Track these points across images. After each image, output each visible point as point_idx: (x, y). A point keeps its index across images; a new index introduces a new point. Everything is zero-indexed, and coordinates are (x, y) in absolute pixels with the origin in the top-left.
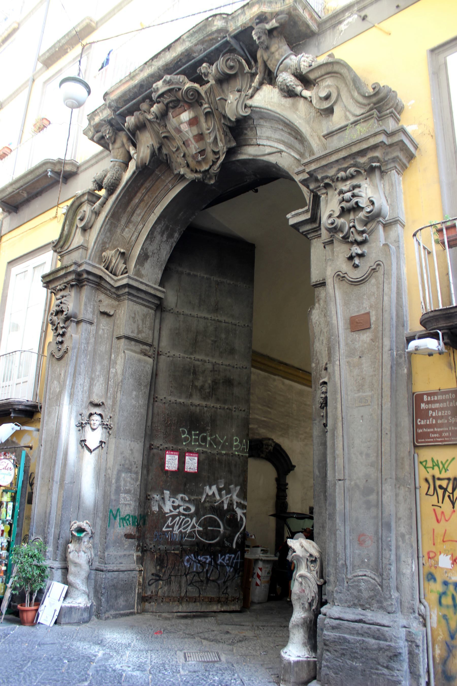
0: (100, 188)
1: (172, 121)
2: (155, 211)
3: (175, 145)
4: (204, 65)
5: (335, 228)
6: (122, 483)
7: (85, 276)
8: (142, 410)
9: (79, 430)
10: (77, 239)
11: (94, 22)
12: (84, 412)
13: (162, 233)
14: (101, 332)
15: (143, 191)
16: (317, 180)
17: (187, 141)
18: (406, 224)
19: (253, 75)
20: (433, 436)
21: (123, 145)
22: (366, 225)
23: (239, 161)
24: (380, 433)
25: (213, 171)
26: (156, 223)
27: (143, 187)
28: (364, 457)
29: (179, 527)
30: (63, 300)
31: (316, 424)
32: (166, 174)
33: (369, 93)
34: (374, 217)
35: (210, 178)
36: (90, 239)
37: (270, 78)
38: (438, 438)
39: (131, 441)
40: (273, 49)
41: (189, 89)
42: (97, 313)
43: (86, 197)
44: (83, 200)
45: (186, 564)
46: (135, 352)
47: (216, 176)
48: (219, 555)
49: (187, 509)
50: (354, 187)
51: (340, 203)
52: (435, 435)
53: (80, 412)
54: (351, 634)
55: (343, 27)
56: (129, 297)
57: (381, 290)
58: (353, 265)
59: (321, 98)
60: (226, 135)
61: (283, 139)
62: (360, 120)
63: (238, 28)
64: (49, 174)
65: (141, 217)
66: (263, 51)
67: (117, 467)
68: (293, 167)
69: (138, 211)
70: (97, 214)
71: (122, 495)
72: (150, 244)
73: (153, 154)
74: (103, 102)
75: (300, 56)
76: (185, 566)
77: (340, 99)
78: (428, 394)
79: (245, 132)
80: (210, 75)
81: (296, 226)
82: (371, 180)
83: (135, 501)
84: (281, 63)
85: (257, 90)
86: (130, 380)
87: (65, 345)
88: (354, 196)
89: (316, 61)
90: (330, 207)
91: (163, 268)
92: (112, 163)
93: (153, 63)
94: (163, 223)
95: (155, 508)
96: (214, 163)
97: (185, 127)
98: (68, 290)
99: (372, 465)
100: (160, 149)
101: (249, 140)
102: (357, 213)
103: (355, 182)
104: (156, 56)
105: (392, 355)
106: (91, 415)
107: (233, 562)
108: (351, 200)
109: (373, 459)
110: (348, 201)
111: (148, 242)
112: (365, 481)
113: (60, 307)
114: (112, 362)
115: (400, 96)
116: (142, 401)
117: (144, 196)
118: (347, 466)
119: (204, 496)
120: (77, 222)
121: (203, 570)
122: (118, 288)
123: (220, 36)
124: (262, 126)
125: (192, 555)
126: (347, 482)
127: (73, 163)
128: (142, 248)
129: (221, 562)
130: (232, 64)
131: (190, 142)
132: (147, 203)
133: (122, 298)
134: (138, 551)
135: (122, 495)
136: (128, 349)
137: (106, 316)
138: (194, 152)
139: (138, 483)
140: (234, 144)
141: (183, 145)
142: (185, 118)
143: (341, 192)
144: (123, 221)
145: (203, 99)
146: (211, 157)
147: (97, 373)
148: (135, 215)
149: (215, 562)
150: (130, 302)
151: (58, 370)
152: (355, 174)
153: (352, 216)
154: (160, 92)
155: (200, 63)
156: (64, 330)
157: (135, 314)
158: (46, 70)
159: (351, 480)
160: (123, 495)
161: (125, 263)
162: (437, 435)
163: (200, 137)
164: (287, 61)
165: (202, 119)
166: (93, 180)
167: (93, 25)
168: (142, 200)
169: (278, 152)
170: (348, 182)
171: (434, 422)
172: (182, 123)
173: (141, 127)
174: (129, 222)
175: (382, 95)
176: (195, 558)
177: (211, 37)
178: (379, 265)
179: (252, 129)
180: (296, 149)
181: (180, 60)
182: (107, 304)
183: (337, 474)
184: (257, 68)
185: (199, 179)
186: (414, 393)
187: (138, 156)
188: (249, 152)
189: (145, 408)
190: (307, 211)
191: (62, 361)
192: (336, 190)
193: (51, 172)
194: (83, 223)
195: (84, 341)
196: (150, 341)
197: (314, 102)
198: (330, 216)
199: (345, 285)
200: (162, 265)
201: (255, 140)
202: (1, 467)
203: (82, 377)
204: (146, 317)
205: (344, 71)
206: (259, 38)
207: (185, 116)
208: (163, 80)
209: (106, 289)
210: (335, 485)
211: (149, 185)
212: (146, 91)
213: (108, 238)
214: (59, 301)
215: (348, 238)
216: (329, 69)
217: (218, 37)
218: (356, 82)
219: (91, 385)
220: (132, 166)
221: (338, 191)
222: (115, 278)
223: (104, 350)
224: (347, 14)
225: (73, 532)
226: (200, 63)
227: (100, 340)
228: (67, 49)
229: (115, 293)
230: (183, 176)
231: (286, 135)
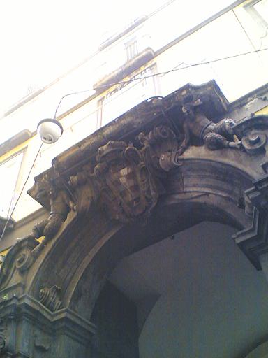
7: (24, 310)
19: (179, 142)
21: (63, 201)
40: (198, 119)
43: (26, 242)
55: (247, 106)
61: (210, 184)
70: (35, 257)
73: (92, 204)
85: (185, 149)
96: (147, 208)
97: (123, 180)
128: (77, 287)
138: (130, 199)
154: (105, 153)
163: (135, 188)
164: (210, 126)
165: (138, 175)
167: (30, 134)
172: (121, 176)
173: (81, 184)
207: (124, 172)
220: (71, 217)
224: (249, 99)
226: (138, 133)
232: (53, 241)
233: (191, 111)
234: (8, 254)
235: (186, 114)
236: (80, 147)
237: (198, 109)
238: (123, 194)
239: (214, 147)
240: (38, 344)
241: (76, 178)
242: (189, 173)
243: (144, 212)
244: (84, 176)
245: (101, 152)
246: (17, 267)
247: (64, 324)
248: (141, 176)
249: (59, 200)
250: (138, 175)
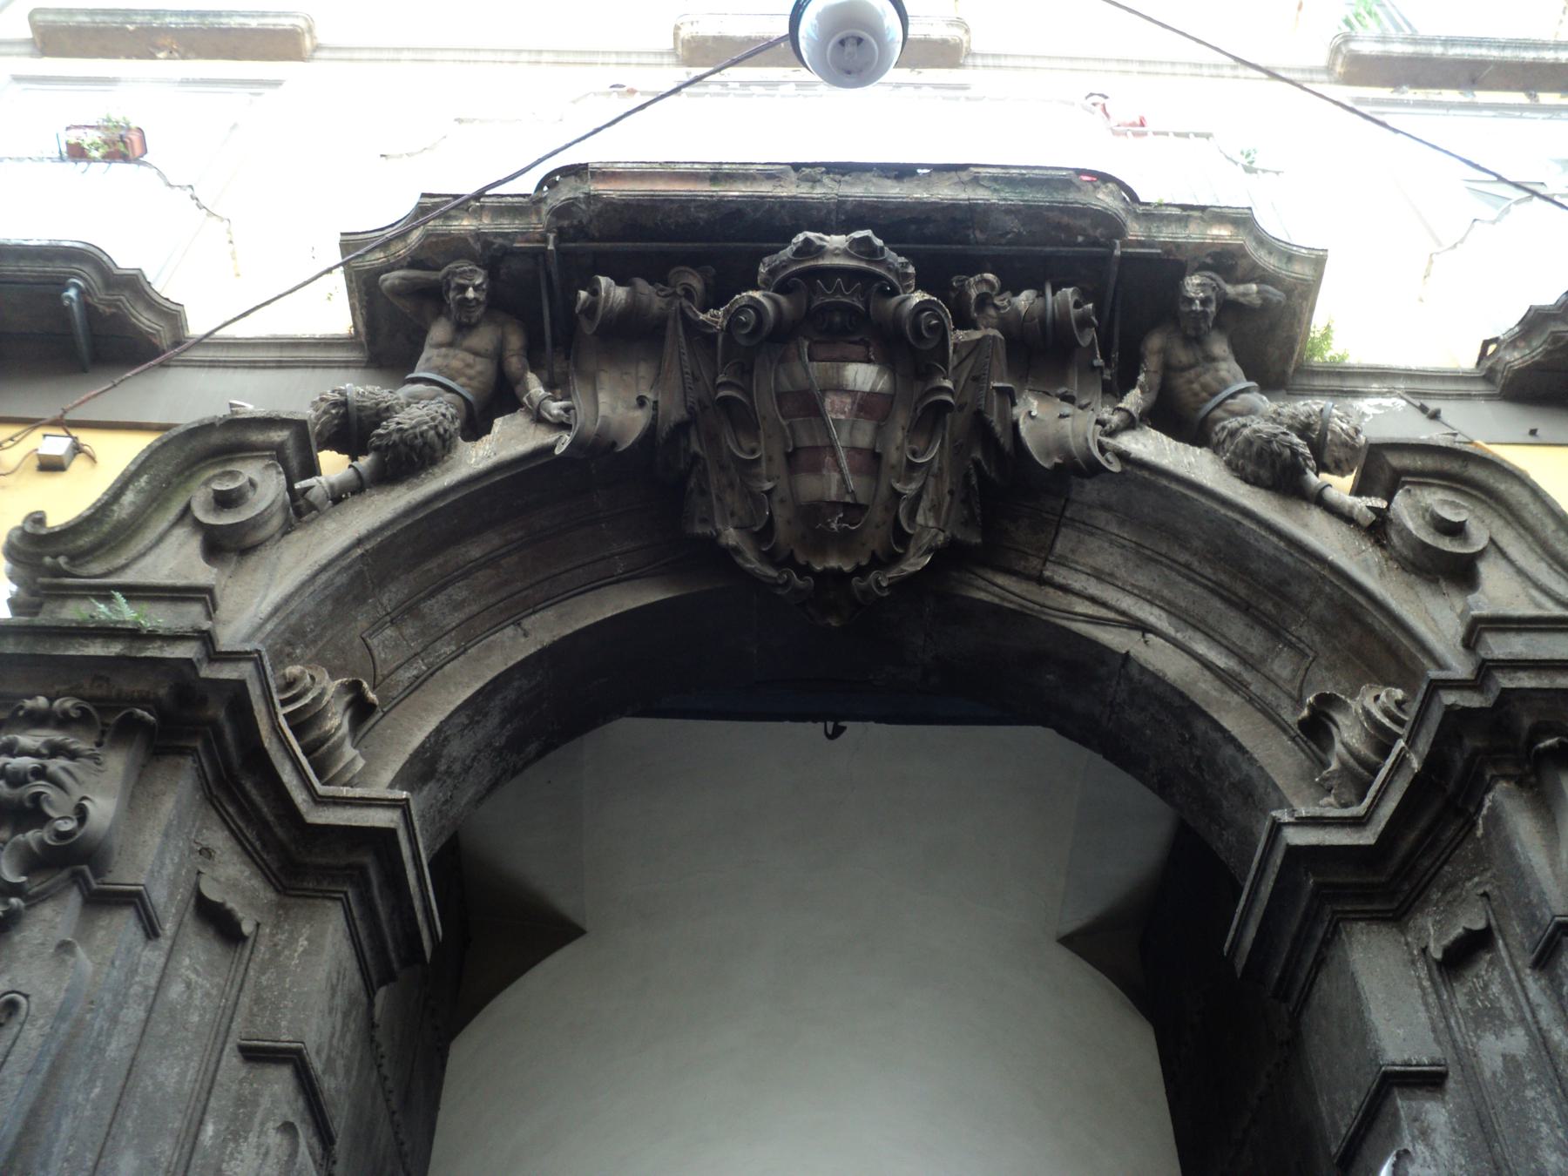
2: (526, 623)
11: (313, 37)
14: (175, 991)
21: (498, 357)
44: (257, 437)
61: (1166, 593)
63: (1151, 246)
64: (72, 293)
69: (458, 592)
73: (651, 432)
84: (1233, 396)
85: (1131, 424)
97: (836, 408)
100: (681, 428)
117: (509, 553)
123: (1091, 232)
124: (1092, 530)
127: (173, 316)
128: (438, 730)
131: (828, 459)
138: (833, 493)
142: (860, 380)
144: (391, 596)
148: (442, 597)
152: (74, 713)
158: (32, 55)
163: (872, 460)
165: (901, 419)
168: (490, 561)
182: (233, 879)
193: (81, 292)
217: (1083, 232)
223: (171, 1085)
224: (1375, 386)
226: (974, 265)
227: (164, 1028)
228: (160, 49)
233: (1212, 308)
239: (1264, 474)
240: (213, 893)
241: (620, 293)
242: (1101, 518)
245: (809, 249)
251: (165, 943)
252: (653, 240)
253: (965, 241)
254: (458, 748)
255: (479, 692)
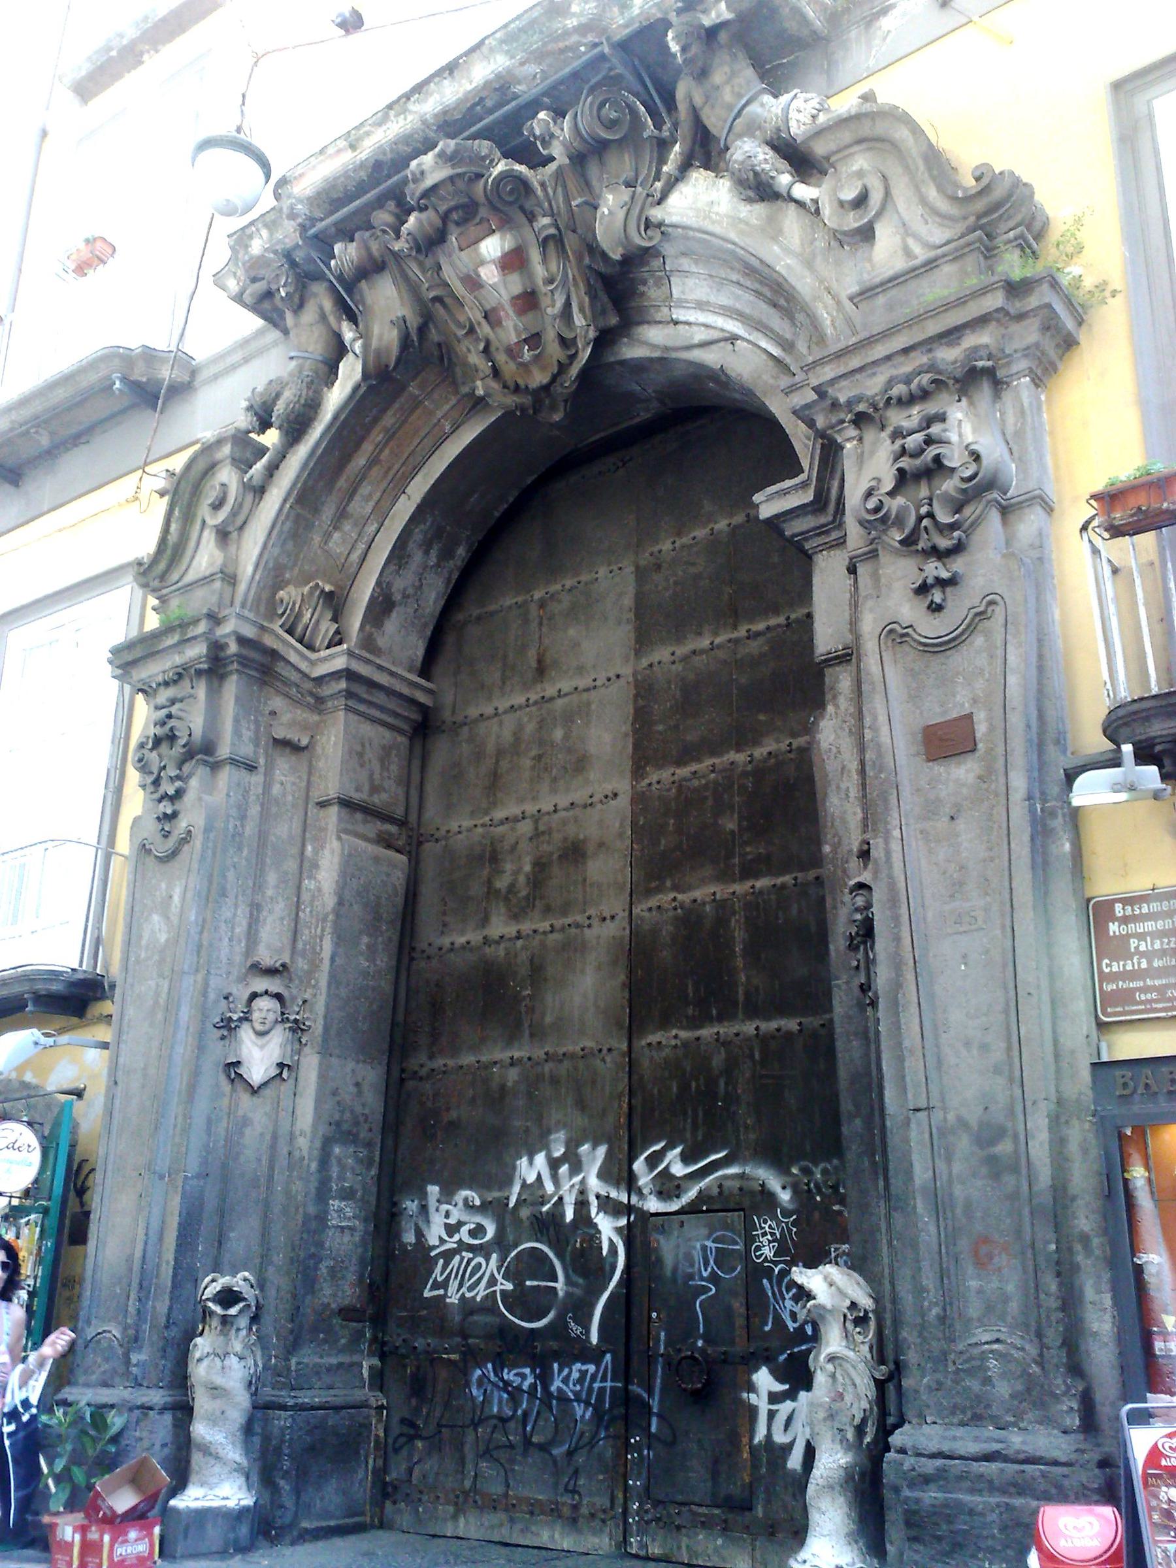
0: (265, 425)
1: (453, 264)
3: (462, 319)
4: (542, 115)
5: (884, 520)
6: (335, 1171)
8: (383, 983)
9: (223, 1038)
10: (205, 557)
12: (234, 991)
13: (427, 546)
14: (276, 790)
15: (377, 436)
16: (835, 405)
17: (494, 309)
18: (1056, 506)
19: (663, 146)
20: (1143, 997)
21: (323, 317)
22: (958, 510)
23: (623, 363)
24: (1012, 993)
25: (559, 390)
26: (412, 519)
27: (378, 428)
28: (975, 1052)
29: (461, 1286)
30: (174, 710)
31: (839, 986)
32: (436, 396)
33: (965, 189)
34: (982, 487)
35: (553, 408)
36: (243, 556)
37: (706, 151)
38: (1156, 1001)
39: (358, 1062)
40: (718, 77)
41: (503, 176)
42: (267, 744)
45: (475, 1392)
46: (366, 839)
47: (566, 401)
48: (556, 1366)
49: (478, 1231)
50: (929, 421)
51: (896, 460)
52: (1149, 996)
53: (225, 992)
54: (972, 1491)
56: (350, 703)
57: (1000, 661)
58: (929, 607)
59: (842, 204)
60: (593, 297)
61: (738, 306)
62: (944, 256)
65: (372, 503)
66: (693, 84)
67: (323, 1129)
68: (765, 377)
69: (365, 489)
70: (260, 491)
71: (335, 1204)
72: (397, 572)
73: (405, 342)
74: (273, 203)
75: (785, 98)
76: (473, 1398)
77: (889, 207)
78: (1126, 901)
79: (642, 288)
80: (555, 143)
81: (774, 523)
82: (971, 404)
83: (366, 1220)
85: (672, 183)
86: (356, 907)
87: (182, 824)
88: (929, 441)
89: (828, 110)
90: (869, 467)
91: (429, 633)
92: (294, 363)
93: (411, 106)
94: (430, 520)
95: (409, 1238)
96: (562, 368)
97: (490, 274)
98: (186, 683)
99: (997, 1070)
100: (422, 330)
101: (652, 310)
102: (936, 482)
103: (931, 408)
104: (419, 88)
105: (1032, 811)
106: (254, 996)
107: (590, 1389)
108: (923, 451)
109: (998, 1054)
110: (916, 454)
111: (393, 568)
112: (981, 1108)
113: (168, 726)
114: (306, 865)
115: (1041, 197)
116: (384, 961)
117: (381, 451)
118: (933, 1075)
119: (516, 1189)
120: (204, 511)
121: (515, 1411)
122: (320, 680)
124: (687, 273)
125: (490, 1366)
126: (937, 1116)
129: (559, 1389)
130: (613, 115)
132: (389, 469)
133: (330, 704)
134: (371, 1354)
135: (335, 1204)
136: (346, 831)
137: (288, 750)
138: (514, 339)
139: (374, 1172)
140: (614, 320)
141: (483, 322)
143: (898, 434)
144: (328, 512)
145: (539, 205)
146: (554, 351)
147: (270, 893)
148: (357, 498)
149: (546, 1388)
150: (351, 715)
151: (163, 886)
153: (924, 492)
154: (429, 182)
155: (533, 107)
156: (178, 784)
157: (363, 745)
159: (945, 1109)
160: (337, 1203)
161: (335, 619)
162: (1154, 996)
163: (528, 301)
164: (754, 108)
165: (535, 255)
166: (245, 404)
168: (374, 461)
169: (726, 340)
170: (915, 410)
171: (1144, 965)
172: (482, 263)
173: (371, 268)
174: (342, 515)
175: (998, 194)
176: (496, 1375)
177: (561, 45)
178: (991, 603)
179: (658, 283)
180: (772, 330)
181: (482, 99)
182: (289, 719)
183: (910, 1096)
184: (676, 125)
185: (523, 409)
186: (1089, 900)
187: (366, 347)
188: (650, 340)
189: (391, 977)
190: (804, 485)
191: (176, 864)
192: (883, 428)
194: (222, 515)
195: (234, 812)
196: (399, 812)
197: (826, 211)
198: (869, 494)
199: (909, 654)
200: (425, 625)
201: (665, 310)
202: (2, 1143)
203: (230, 901)
204: (388, 755)
205: (902, 134)
206: (684, 50)
207: (492, 247)
208: (437, 150)
209: (287, 683)
210: (907, 1123)
211: (392, 421)
212: (389, 177)
213: (289, 556)
214: (164, 712)
215: (915, 543)
216: (866, 129)
218: (936, 163)
219: (254, 923)
221: (889, 430)
222: (313, 656)
225: (210, 1304)
226: (533, 107)
229: (311, 694)
230: (481, 399)
231: (749, 297)
232: (303, 450)
234: (189, 467)
235: (680, 60)
236: (353, 147)
237: (723, 36)
238: (489, 316)
240: (280, 733)
243: (554, 378)
244: (375, 247)
246: (211, 522)
247: (343, 685)
248: (545, 260)
249: (309, 315)
250: (535, 255)
251: (262, 770)
252: (351, 202)
253: (516, 97)
254: (401, 583)
255: (392, 551)
